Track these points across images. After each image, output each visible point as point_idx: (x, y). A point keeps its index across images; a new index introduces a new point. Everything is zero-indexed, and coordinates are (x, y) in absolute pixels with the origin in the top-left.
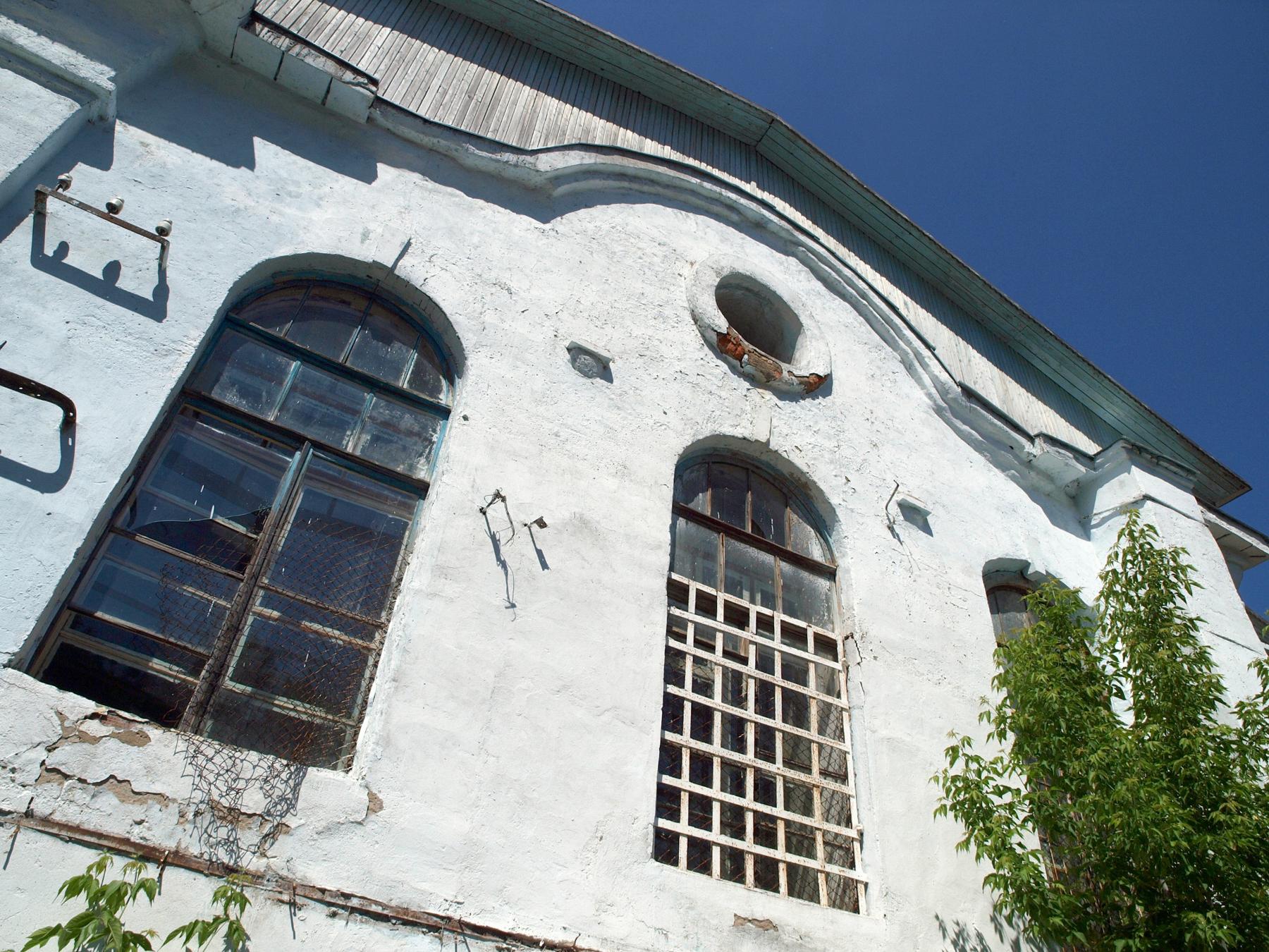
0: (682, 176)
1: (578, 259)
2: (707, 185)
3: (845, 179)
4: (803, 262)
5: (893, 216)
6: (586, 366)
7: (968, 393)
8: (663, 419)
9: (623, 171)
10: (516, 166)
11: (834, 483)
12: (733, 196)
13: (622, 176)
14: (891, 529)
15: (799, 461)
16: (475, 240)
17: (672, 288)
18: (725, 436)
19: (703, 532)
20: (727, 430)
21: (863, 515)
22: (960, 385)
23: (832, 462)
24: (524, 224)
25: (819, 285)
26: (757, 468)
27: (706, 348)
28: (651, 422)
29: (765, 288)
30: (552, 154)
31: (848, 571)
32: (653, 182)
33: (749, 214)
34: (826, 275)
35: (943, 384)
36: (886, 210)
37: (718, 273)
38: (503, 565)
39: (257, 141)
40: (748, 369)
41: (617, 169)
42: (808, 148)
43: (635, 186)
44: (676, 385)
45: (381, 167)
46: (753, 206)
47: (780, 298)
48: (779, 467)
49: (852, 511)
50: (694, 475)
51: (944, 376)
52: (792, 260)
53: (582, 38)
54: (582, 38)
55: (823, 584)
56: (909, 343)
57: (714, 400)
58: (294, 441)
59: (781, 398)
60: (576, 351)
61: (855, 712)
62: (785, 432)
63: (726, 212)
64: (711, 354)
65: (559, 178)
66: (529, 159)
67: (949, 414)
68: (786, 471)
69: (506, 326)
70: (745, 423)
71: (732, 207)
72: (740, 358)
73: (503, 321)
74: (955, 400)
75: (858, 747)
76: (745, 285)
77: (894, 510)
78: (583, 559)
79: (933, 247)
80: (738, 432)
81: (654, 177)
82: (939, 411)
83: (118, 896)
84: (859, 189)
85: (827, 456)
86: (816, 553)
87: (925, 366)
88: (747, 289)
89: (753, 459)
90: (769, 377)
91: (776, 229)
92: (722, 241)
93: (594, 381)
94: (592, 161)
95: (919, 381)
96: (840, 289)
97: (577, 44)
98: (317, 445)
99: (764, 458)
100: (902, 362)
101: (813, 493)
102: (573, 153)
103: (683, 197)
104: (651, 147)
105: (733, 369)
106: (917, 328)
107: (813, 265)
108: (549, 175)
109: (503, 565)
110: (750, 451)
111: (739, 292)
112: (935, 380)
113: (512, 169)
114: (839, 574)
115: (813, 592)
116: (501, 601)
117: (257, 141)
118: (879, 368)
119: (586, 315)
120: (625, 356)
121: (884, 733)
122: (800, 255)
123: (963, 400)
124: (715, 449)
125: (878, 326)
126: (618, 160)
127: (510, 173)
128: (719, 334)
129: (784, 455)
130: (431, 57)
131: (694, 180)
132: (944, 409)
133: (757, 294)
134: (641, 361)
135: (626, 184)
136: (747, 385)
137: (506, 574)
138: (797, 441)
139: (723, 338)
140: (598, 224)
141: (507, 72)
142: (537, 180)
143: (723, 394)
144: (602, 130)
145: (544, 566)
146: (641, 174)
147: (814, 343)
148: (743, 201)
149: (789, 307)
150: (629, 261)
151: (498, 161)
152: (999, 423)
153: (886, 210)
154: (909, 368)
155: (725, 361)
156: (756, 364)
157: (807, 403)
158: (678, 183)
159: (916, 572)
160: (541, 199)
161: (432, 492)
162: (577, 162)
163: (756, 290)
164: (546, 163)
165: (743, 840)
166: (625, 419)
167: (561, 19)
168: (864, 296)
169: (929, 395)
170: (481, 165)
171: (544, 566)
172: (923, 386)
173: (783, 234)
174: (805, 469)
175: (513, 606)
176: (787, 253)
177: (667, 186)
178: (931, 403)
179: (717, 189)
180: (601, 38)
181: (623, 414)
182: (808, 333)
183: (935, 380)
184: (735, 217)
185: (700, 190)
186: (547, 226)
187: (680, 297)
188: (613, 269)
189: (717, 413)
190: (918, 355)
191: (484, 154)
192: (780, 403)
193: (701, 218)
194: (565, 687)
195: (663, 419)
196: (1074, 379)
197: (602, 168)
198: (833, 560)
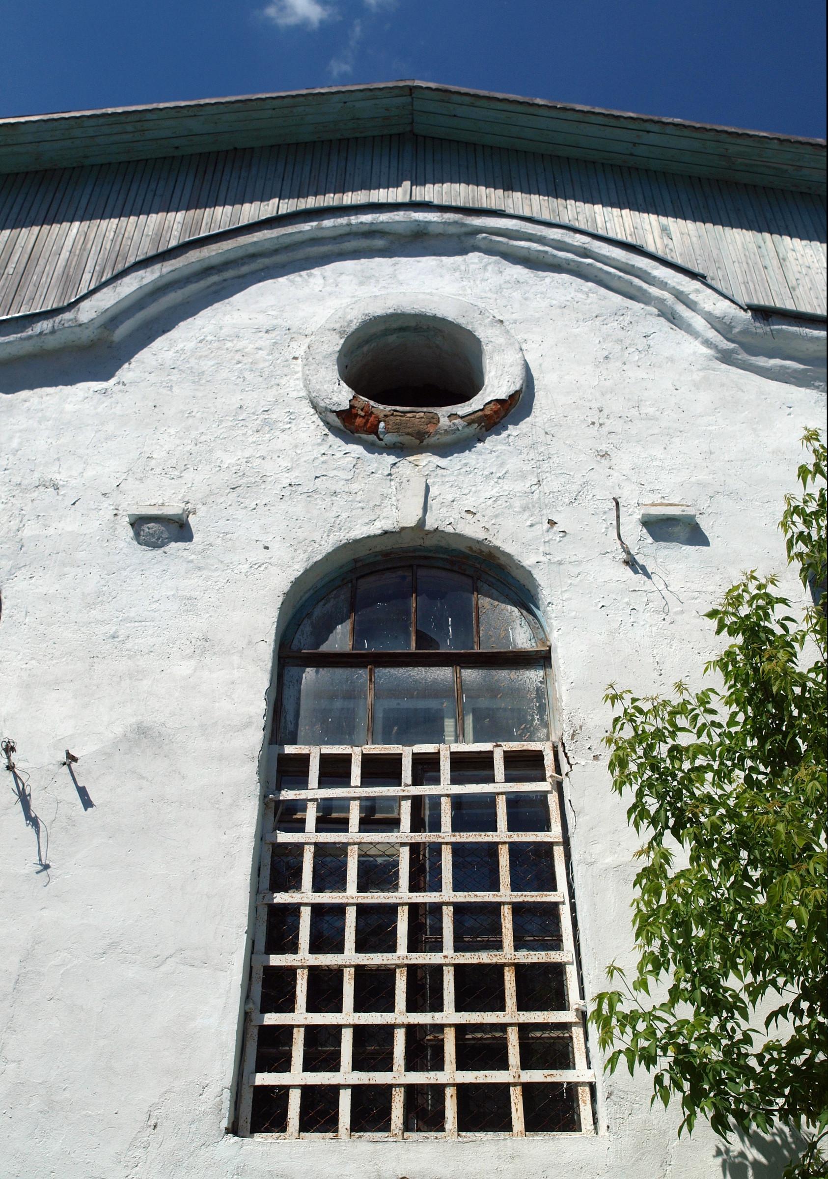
0: (290, 229)
1: (152, 404)
2: (328, 223)
3: (531, 110)
4: (489, 252)
5: (613, 122)
6: (152, 535)
7: (763, 313)
8: (261, 556)
9: (205, 264)
10: (53, 332)
11: (530, 534)
12: (367, 218)
13: (208, 270)
14: (631, 563)
15: (472, 530)
16: (15, 444)
17: (283, 381)
18: (356, 542)
19: (340, 673)
20: (360, 531)
21: (579, 562)
22: (751, 308)
23: (525, 509)
24: (77, 398)
25: (519, 272)
26: (426, 558)
27: (331, 437)
28: (245, 568)
29: (434, 318)
30: (98, 295)
32: (253, 256)
33: (400, 229)
34: (524, 253)
35: (720, 319)
36: (601, 120)
37: (341, 333)
38: (34, 822)
40: (389, 438)
41: (197, 267)
42: (467, 99)
43: (230, 274)
44: (283, 506)
46: (399, 216)
47: (443, 320)
48: (454, 546)
49: (560, 563)
50: (328, 606)
51: (722, 307)
52: (474, 258)
53: (129, 128)
54: (129, 128)
55: (533, 676)
56: (663, 285)
57: (339, 501)
59: (444, 455)
60: (138, 522)
62: (450, 498)
63: (364, 243)
64: (338, 442)
65: (114, 319)
66: (67, 316)
67: (743, 356)
68: (462, 547)
69: (51, 531)
71: (371, 232)
72: (374, 430)
73: (46, 526)
74: (745, 332)
76: (395, 325)
77: (633, 532)
78: (142, 777)
79: (686, 132)
80: (376, 529)
81: (252, 250)
82: (726, 358)
84: (554, 113)
85: (517, 504)
86: (522, 638)
87: (691, 305)
88: (402, 329)
89: (415, 549)
90: (421, 435)
91: (439, 229)
92: (361, 283)
93: (166, 549)
94: (156, 275)
95: (688, 328)
96: (550, 260)
97: (126, 137)
99: (429, 542)
100: (662, 314)
102: (126, 280)
103: (300, 254)
104: (250, 212)
105: (371, 448)
107: (503, 249)
108: (97, 323)
109: (34, 822)
110: (407, 542)
111: (392, 339)
113: (51, 338)
115: (516, 692)
116: (31, 866)
118: (619, 341)
119: (158, 470)
120: (210, 500)
122: (482, 245)
123: (760, 328)
124: (355, 561)
125: (615, 284)
126: (194, 256)
127: (52, 343)
128: (339, 414)
129: (449, 529)
130: (131, 228)
131: (307, 227)
132: (732, 351)
133: (417, 329)
134: (233, 495)
135: (215, 278)
136: (392, 459)
137: (38, 833)
138: (469, 503)
139: (347, 416)
140: (180, 346)
141: (122, 212)
142: (86, 335)
143: (355, 487)
144: (173, 225)
145: (87, 804)
146: (232, 256)
147: (496, 358)
148: (384, 217)
149: (458, 327)
150: (224, 374)
151: (30, 337)
153: (601, 120)
154: (673, 318)
155: (358, 442)
156: (398, 429)
157: (491, 441)
158: (288, 240)
159: (675, 607)
160: (96, 356)
162: (135, 286)
163: (413, 324)
164: (88, 312)
166: (207, 579)
167: (92, 122)
168: (585, 253)
169: (707, 343)
170: (14, 351)
171: (87, 804)
172: (695, 334)
173: (452, 230)
175: (46, 867)
176: (463, 252)
177: (276, 251)
178: (705, 350)
179: (343, 221)
180: (149, 116)
181: (205, 573)
184: (379, 243)
185: (320, 234)
186: (113, 381)
187: (294, 386)
188: (199, 394)
189: (344, 515)
190: (680, 297)
191: (12, 337)
192: (443, 462)
193: (329, 269)
194: (113, 945)
195: (263, 556)
197: (176, 275)
198: (544, 640)
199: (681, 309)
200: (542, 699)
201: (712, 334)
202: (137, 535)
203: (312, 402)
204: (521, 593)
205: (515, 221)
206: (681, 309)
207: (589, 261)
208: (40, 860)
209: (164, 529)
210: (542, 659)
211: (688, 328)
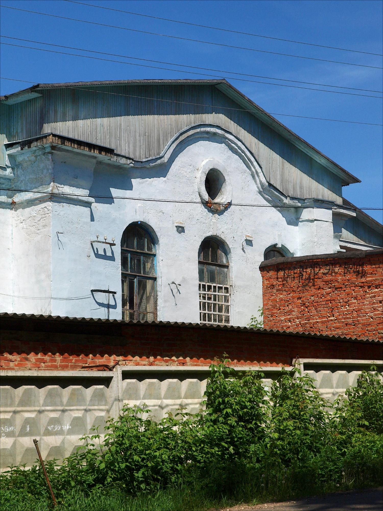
7: (270, 185)
31: (232, 267)
39: (110, 188)
45: (133, 181)
55: (226, 270)
56: (254, 168)
58: (135, 276)
61: (231, 306)
67: (263, 193)
68: (219, 239)
70: (211, 230)
71: (208, 133)
75: (232, 315)
82: (260, 192)
83: (212, 382)
87: (258, 176)
90: (217, 210)
95: (256, 182)
98: (138, 276)
101: (225, 244)
106: (258, 160)
109: (174, 295)
112: (261, 182)
114: (230, 267)
116: (174, 304)
117: (110, 188)
121: (237, 311)
138: (222, 230)
152: (277, 194)
154: (253, 177)
161: (157, 279)
165: (8, 155)
168: (243, 152)
169: (258, 187)
172: (256, 184)
174: (224, 239)
178: (257, 189)
182: (227, 183)
183: (261, 182)
196: (308, 151)
199: (256, 176)
200: (226, 276)
201: (260, 186)
202: (177, 230)
203: (199, 193)
204: (226, 252)
205: (233, 137)
206: (256, 176)
207: (243, 154)
208: (113, 296)
209: (180, 229)
210: (227, 267)
211: (256, 182)
